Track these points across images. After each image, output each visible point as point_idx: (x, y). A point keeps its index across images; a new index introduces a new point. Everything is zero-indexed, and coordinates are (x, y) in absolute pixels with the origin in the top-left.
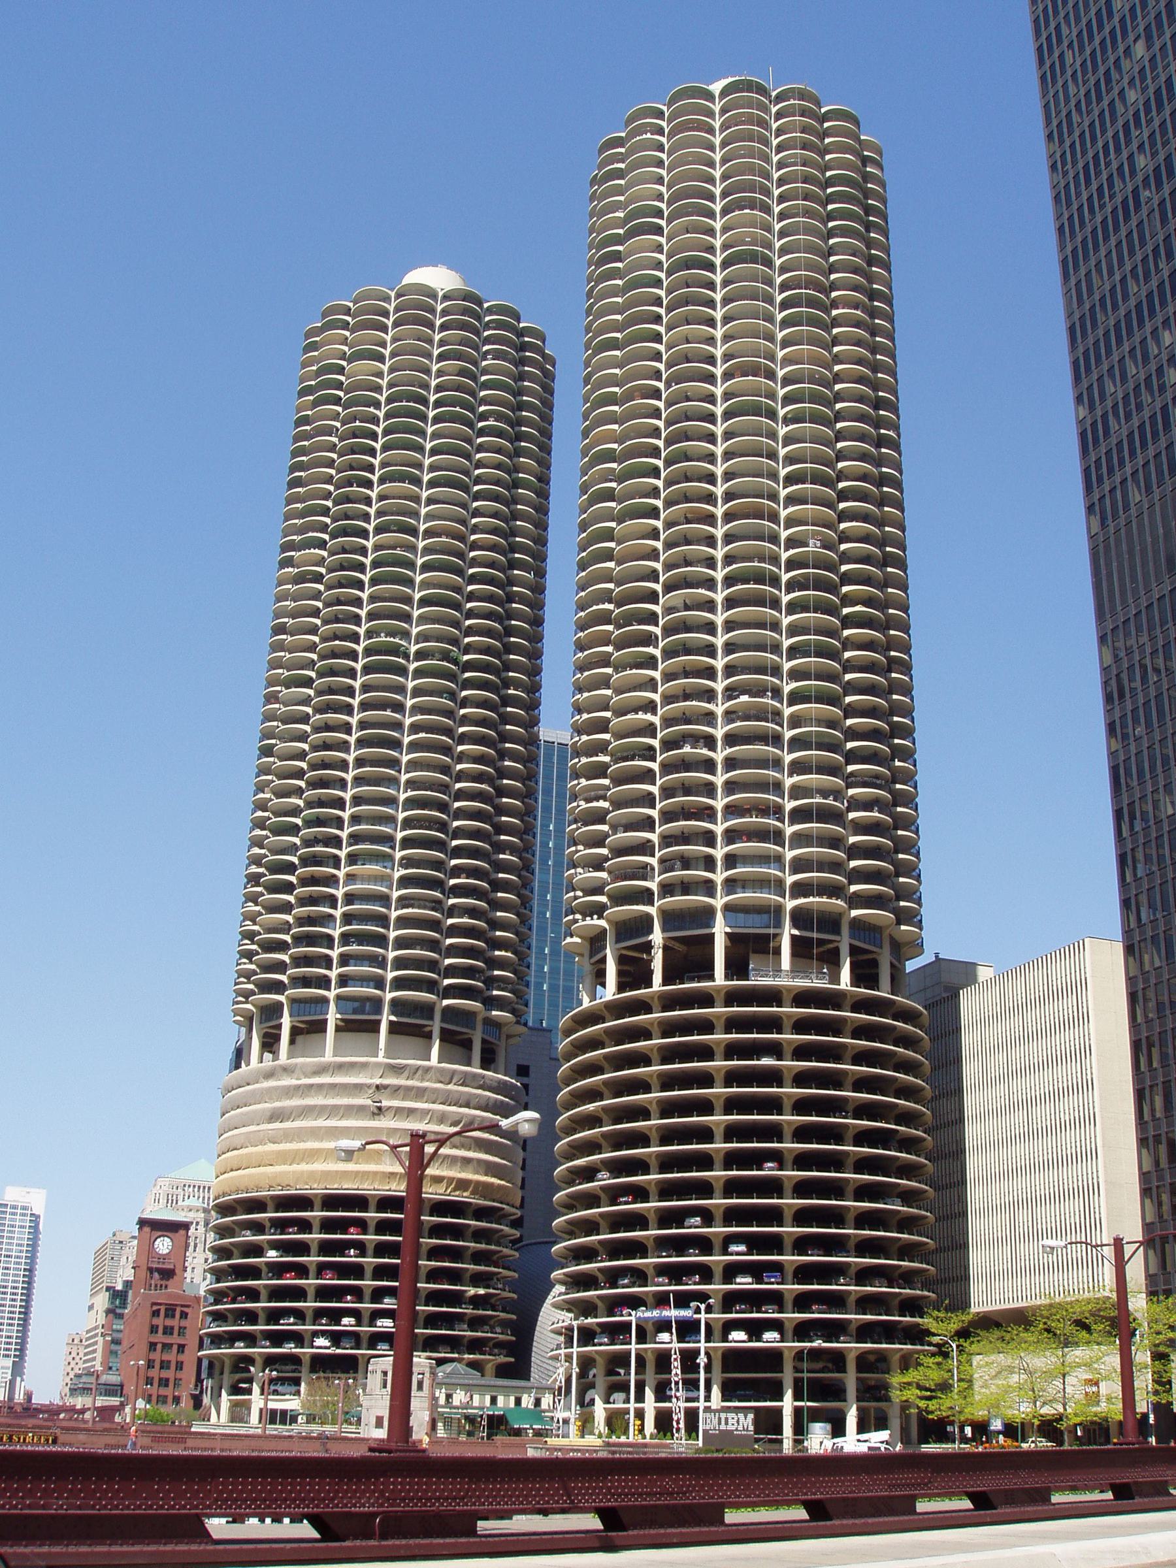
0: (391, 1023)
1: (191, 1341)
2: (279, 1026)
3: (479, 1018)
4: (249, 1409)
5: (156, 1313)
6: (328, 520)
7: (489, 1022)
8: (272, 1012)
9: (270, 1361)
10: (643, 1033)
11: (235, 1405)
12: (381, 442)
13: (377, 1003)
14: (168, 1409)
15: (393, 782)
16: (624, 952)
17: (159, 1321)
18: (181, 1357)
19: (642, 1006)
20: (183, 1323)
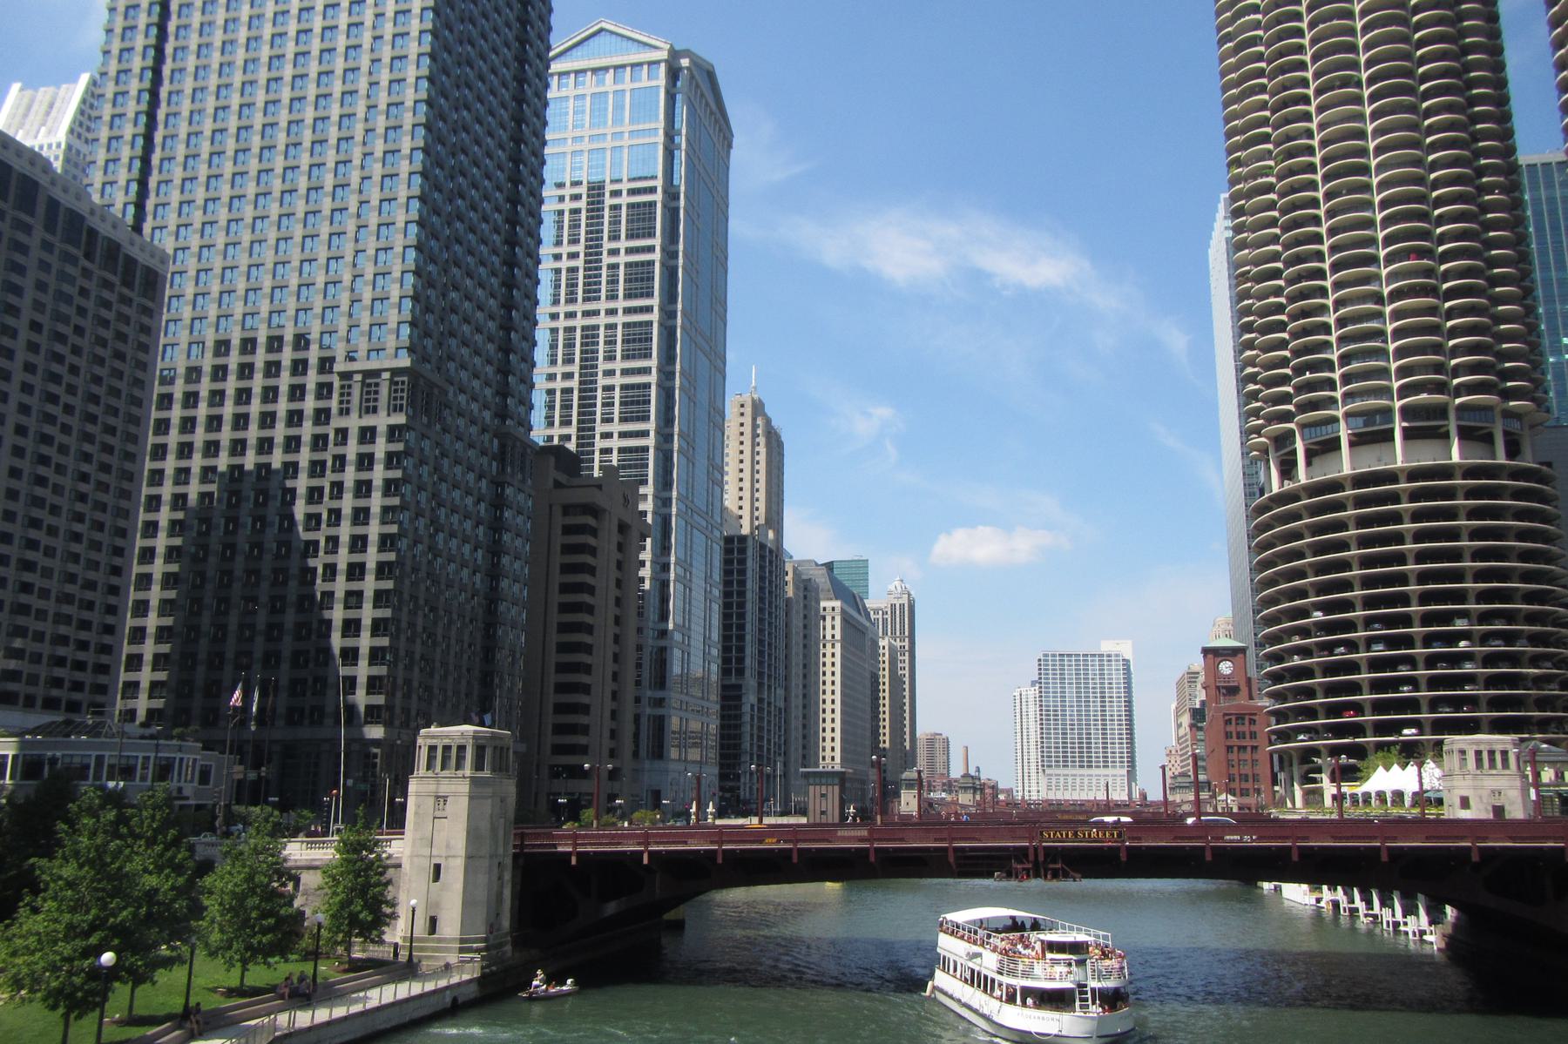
0: (1404, 429)
1: (1261, 741)
2: (1294, 452)
3: (1498, 410)
4: (1322, 795)
5: (1228, 722)
6: (1263, 65)
7: (1508, 414)
8: (1283, 440)
9: (1335, 751)
11: (1307, 794)
12: (1312, 87)
13: (1387, 412)
14: (1251, 800)
15: (1368, 205)
17: (1232, 728)
18: (1253, 728)
20: (1253, 728)
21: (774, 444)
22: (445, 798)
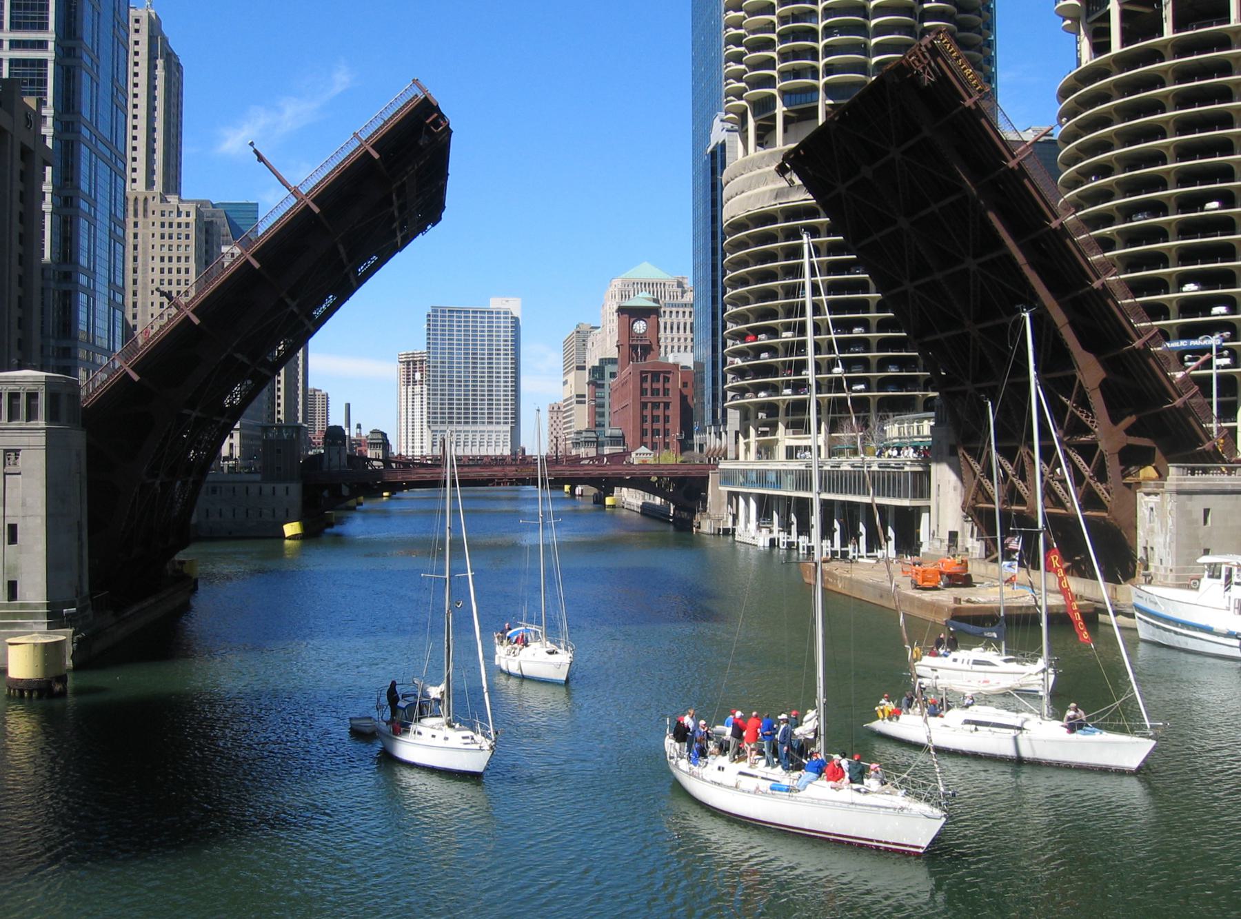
2: (774, 118)
10: (1155, 81)
16: (1098, 25)
19: (1154, 55)
21: (174, 68)
22: (17, 452)
